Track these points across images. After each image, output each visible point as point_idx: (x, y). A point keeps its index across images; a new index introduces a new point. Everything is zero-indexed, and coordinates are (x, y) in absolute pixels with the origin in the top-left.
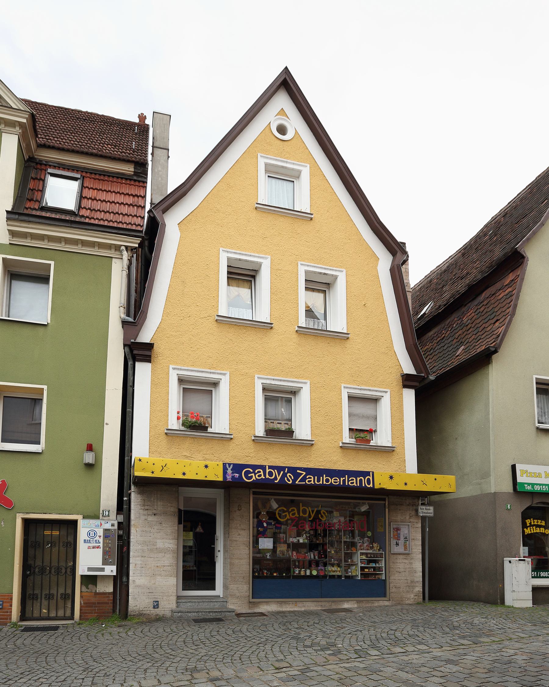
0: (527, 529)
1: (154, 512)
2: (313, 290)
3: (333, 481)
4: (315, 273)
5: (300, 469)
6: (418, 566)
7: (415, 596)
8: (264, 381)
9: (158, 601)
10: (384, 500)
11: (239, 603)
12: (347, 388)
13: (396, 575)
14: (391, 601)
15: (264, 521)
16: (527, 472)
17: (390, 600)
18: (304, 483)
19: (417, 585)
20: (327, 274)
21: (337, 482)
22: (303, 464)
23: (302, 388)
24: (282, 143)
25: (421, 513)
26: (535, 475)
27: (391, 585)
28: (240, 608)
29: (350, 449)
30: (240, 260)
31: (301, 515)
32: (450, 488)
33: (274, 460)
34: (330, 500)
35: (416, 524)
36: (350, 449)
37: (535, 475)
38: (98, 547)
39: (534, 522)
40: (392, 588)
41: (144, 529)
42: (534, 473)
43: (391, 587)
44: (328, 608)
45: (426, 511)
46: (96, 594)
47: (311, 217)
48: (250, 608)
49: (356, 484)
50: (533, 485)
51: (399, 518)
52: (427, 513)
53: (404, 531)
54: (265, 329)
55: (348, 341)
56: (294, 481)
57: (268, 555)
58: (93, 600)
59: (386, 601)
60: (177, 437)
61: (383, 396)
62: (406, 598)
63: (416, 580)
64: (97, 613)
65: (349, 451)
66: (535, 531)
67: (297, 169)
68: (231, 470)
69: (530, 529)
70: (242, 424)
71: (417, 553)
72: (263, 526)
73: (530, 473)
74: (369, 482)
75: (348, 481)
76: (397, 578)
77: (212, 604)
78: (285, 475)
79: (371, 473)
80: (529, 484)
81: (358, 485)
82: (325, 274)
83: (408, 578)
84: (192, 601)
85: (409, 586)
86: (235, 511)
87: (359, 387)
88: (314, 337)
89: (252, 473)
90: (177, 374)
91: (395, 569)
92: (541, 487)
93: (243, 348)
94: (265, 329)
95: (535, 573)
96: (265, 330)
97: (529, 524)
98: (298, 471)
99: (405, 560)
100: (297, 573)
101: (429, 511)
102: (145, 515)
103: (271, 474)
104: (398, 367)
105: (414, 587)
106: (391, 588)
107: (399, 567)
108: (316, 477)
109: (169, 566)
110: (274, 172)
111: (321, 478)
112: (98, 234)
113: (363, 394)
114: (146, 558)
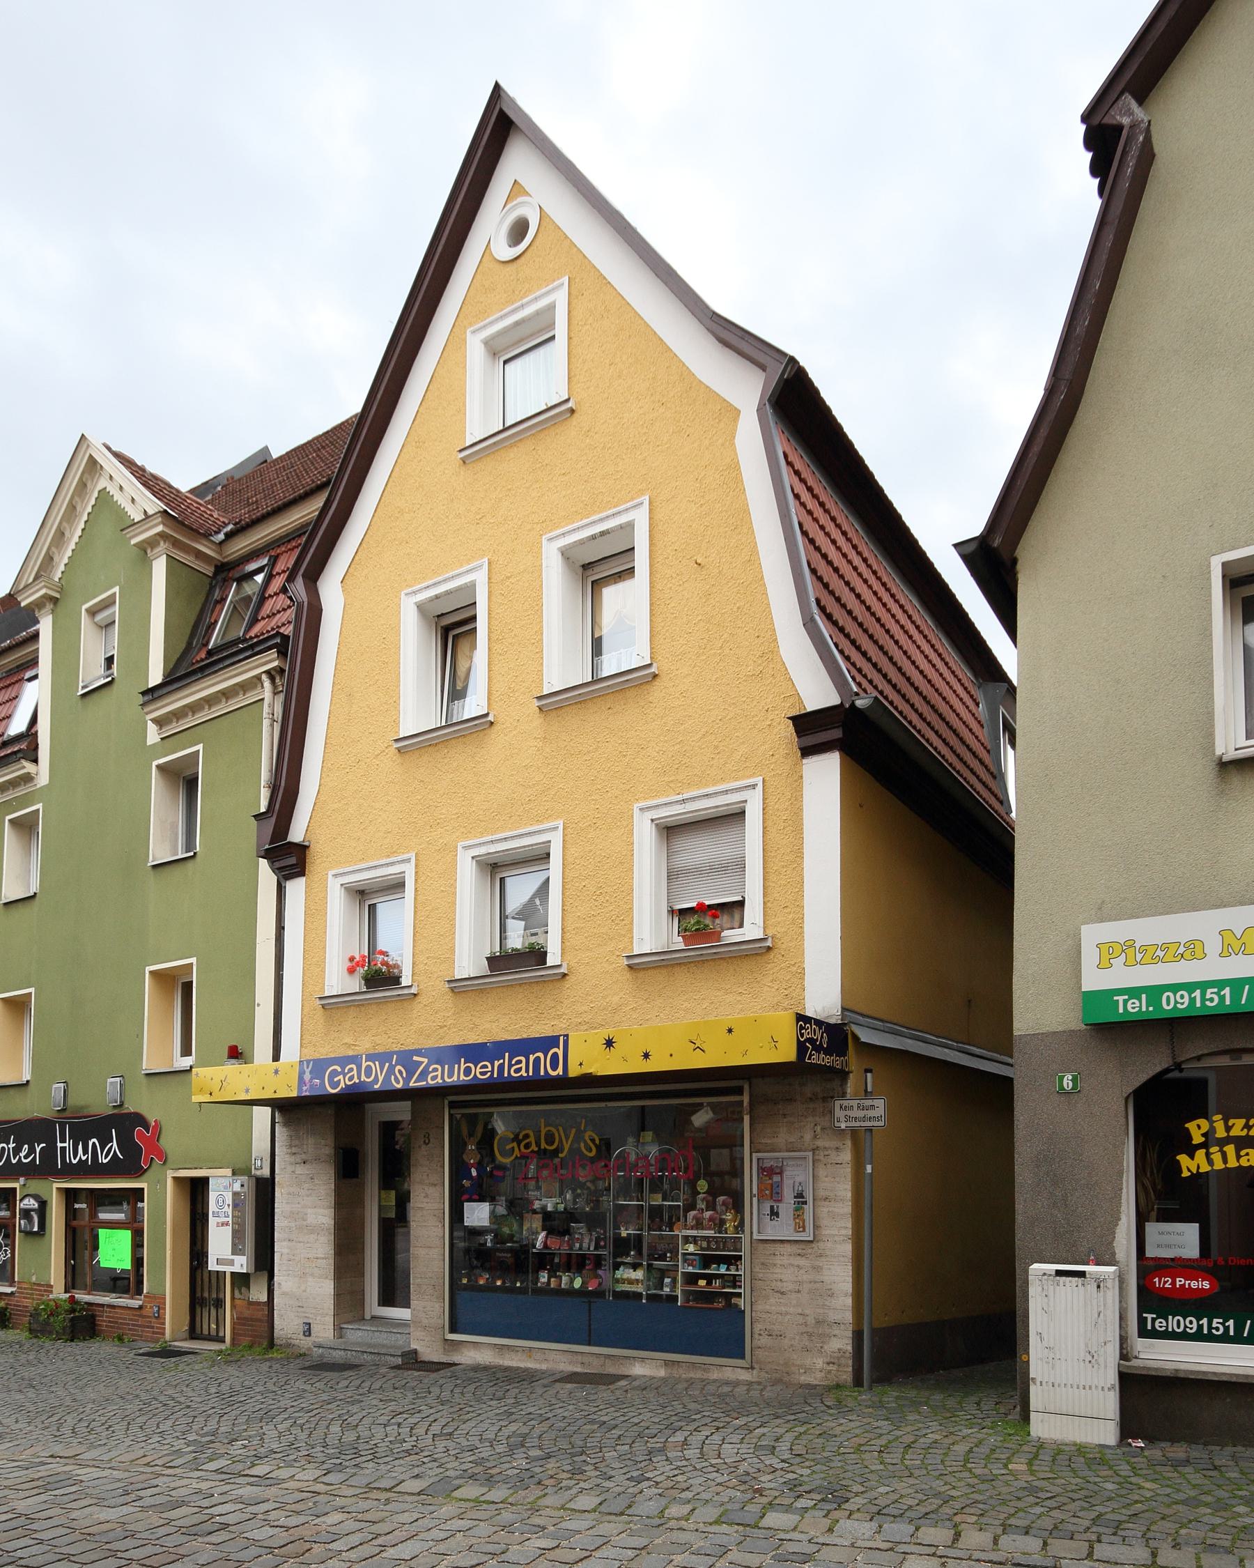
0: (1192, 1158)
1: (304, 1156)
2: (620, 577)
3: (478, 1070)
4: (581, 542)
5: (418, 1052)
6: (840, 1277)
7: (828, 1363)
8: (476, 852)
9: (310, 1324)
10: (740, 1091)
11: (427, 1339)
12: (649, 808)
13: (772, 1300)
14: (755, 1372)
15: (473, 1165)
16: (1130, 946)
17: (752, 1368)
18: (425, 1083)
19: (836, 1332)
20: (608, 530)
21: (486, 1073)
22: (543, 1027)
23: (550, 841)
24: (515, 265)
25: (843, 1119)
26: (1172, 952)
27: (758, 1327)
28: (428, 1350)
29: (653, 968)
30: (437, 597)
31: (542, 1147)
32: (774, 1049)
33: (488, 1026)
34: (603, 1105)
35: (833, 1154)
36: (653, 968)
37: (1172, 952)
38: (227, 1224)
39: (1228, 1129)
40: (760, 1335)
41: (292, 1190)
42: (1165, 947)
43: (756, 1331)
44: (595, 1372)
45: (861, 1114)
46: (251, 1303)
47: (568, 409)
48: (446, 1351)
49: (527, 1071)
50: (1155, 992)
51: (783, 1138)
52: (864, 1119)
53: (795, 1176)
54: (480, 731)
55: (657, 682)
56: (407, 1080)
57: (489, 1240)
58: (247, 1313)
59: (743, 1371)
60: (338, 1008)
61: (746, 801)
62: (800, 1366)
63: (833, 1316)
64: (251, 1336)
65: (650, 972)
66: (1232, 1163)
67: (545, 306)
68: (311, 1072)
69: (1208, 1155)
70: (434, 958)
71: (836, 1238)
72: (470, 1177)
73: (1144, 950)
74: (554, 1066)
75: (510, 1066)
76: (773, 1308)
77: (393, 1337)
78: (391, 1071)
79: (562, 1038)
80: (1134, 992)
81: (531, 1074)
82: (603, 534)
83: (807, 1312)
84: (394, 1331)
85: (810, 1335)
86: (420, 1147)
87: (680, 797)
88: (579, 706)
89: (339, 1074)
90: (652, 820)
91: (768, 1283)
92: (1197, 993)
93: (441, 792)
94: (480, 731)
95: (1231, 1323)
96: (481, 734)
97: (1203, 1135)
98: (415, 1058)
99: (799, 1257)
100: (544, 1283)
101: (871, 1113)
102: (292, 1164)
103: (369, 1071)
104: (791, 700)
105: (824, 1337)
106: (756, 1336)
107: (780, 1276)
108: (446, 1066)
109: (323, 1258)
110: (539, 332)
111: (456, 1066)
112: (231, 671)
113: (692, 812)
114: (294, 1243)
